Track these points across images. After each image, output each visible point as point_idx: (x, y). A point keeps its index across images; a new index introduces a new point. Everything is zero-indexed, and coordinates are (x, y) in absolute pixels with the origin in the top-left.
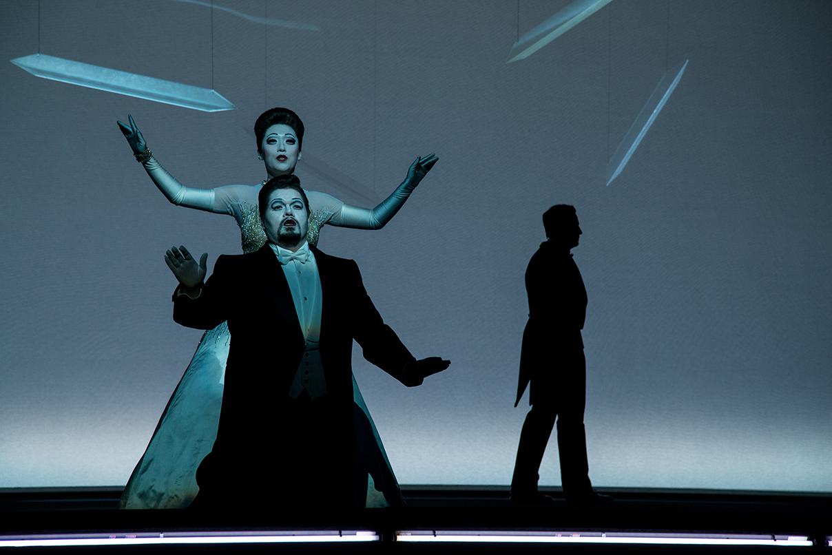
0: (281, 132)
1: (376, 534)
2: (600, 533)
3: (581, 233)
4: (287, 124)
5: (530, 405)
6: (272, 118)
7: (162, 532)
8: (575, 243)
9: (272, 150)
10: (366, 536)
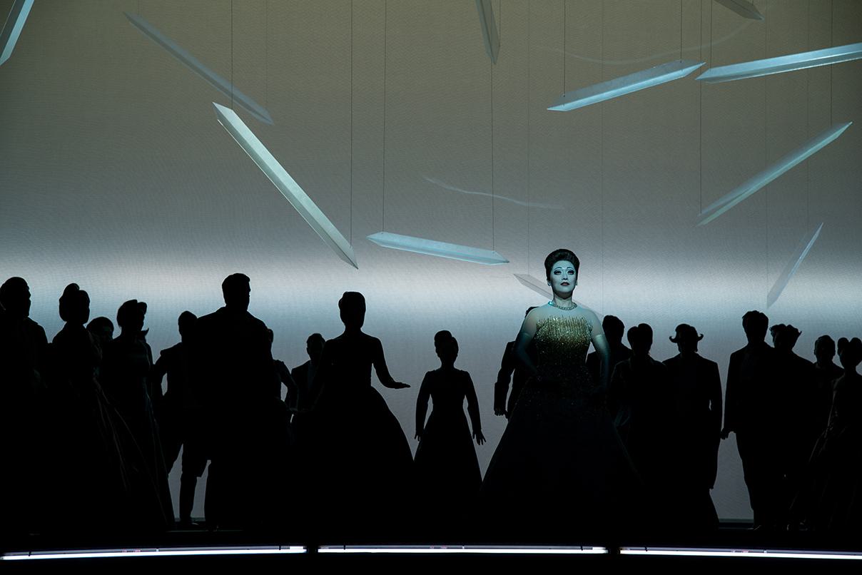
0: (564, 265)
2: (154, 549)
4: (568, 260)
5: (146, 332)
6: (557, 256)
9: (558, 278)
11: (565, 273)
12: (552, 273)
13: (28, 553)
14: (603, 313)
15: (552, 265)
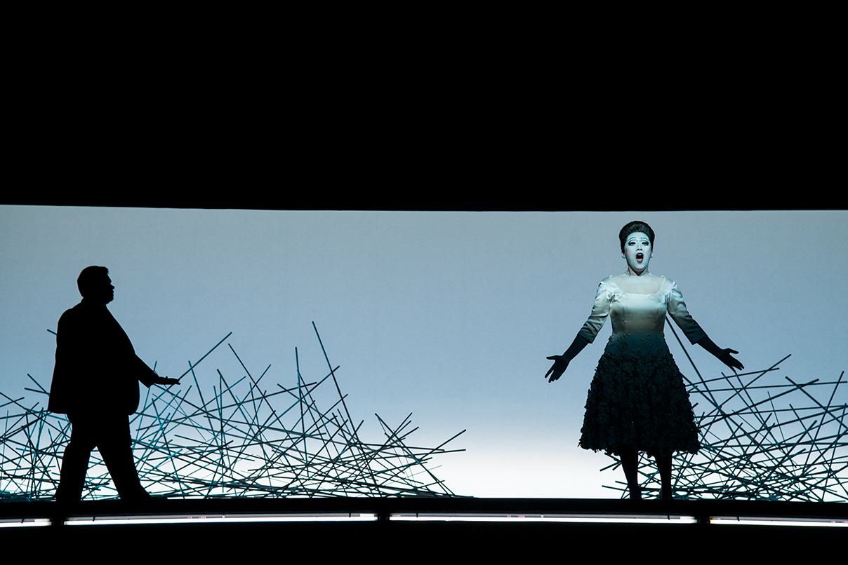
0: (638, 237)
2: (220, 516)
3: (114, 287)
4: (642, 232)
7: (542, 514)
8: (110, 297)
10: (42, 522)
11: (639, 244)
12: (627, 246)
13: (21, 520)
14: (632, 276)
15: (626, 237)
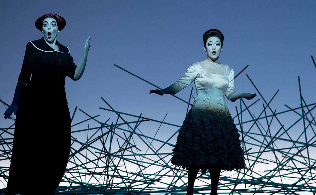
0: (214, 40)
1: (204, 172)
5: (177, 138)
6: (210, 33)
